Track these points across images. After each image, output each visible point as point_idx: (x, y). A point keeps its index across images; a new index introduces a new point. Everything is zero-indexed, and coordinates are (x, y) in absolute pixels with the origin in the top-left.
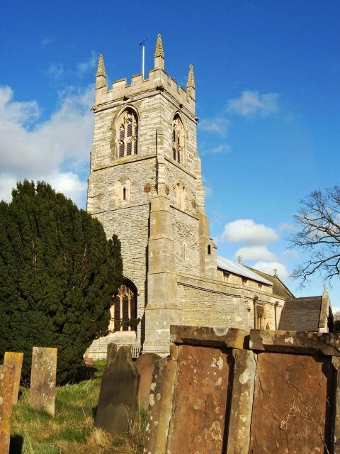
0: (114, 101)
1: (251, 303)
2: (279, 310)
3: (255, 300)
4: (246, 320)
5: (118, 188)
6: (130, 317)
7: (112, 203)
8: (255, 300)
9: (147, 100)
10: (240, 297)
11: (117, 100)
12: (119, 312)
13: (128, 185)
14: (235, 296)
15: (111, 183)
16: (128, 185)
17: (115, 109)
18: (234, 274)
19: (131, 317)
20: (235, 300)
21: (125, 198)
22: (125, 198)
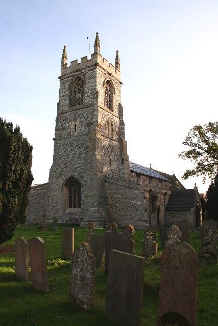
0: (72, 72)
1: (147, 195)
2: (167, 198)
3: (150, 191)
4: (143, 203)
5: (72, 124)
6: (73, 250)
7: (69, 134)
8: (150, 191)
9: (89, 72)
10: (139, 190)
11: (72, 72)
12: (78, 201)
13: (78, 123)
14: (137, 189)
15: (69, 122)
16: (78, 123)
17: (71, 78)
18: (143, 175)
19: (11, 256)
20: (136, 191)
21: (75, 131)
22: (75, 131)
